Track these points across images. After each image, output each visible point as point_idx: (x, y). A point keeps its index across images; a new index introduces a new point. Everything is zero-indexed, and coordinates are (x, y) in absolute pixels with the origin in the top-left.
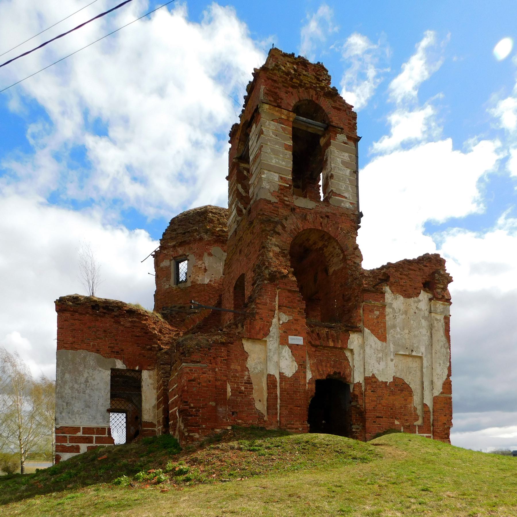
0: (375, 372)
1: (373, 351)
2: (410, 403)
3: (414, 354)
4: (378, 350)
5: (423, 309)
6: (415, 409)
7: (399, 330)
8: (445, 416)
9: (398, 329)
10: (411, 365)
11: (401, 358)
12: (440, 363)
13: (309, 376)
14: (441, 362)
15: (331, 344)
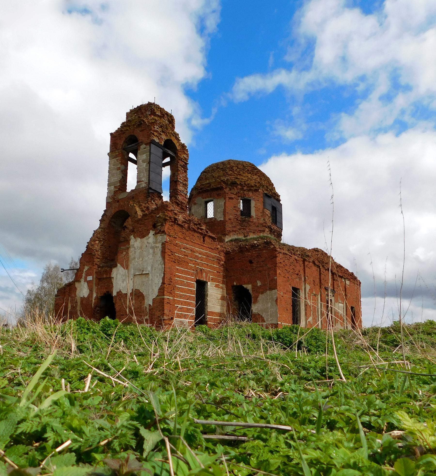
0: (121, 288)
1: (121, 276)
2: (144, 304)
3: (144, 272)
4: (123, 275)
5: (151, 242)
6: (146, 308)
7: (137, 260)
8: (160, 311)
9: (136, 259)
10: (144, 280)
11: (139, 276)
12: (157, 276)
13: (95, 295)
14: (158, 275)
15: (105, 276)
